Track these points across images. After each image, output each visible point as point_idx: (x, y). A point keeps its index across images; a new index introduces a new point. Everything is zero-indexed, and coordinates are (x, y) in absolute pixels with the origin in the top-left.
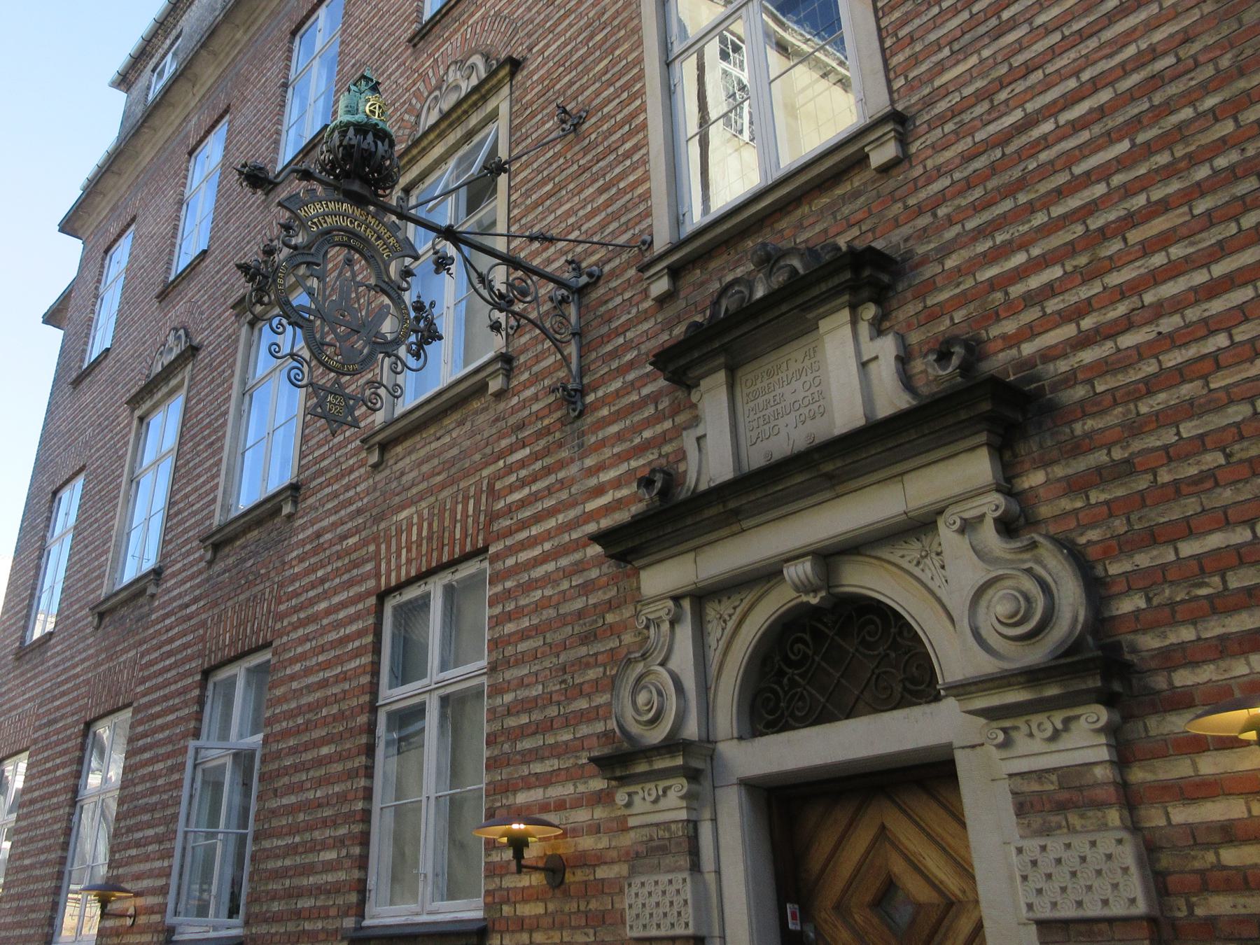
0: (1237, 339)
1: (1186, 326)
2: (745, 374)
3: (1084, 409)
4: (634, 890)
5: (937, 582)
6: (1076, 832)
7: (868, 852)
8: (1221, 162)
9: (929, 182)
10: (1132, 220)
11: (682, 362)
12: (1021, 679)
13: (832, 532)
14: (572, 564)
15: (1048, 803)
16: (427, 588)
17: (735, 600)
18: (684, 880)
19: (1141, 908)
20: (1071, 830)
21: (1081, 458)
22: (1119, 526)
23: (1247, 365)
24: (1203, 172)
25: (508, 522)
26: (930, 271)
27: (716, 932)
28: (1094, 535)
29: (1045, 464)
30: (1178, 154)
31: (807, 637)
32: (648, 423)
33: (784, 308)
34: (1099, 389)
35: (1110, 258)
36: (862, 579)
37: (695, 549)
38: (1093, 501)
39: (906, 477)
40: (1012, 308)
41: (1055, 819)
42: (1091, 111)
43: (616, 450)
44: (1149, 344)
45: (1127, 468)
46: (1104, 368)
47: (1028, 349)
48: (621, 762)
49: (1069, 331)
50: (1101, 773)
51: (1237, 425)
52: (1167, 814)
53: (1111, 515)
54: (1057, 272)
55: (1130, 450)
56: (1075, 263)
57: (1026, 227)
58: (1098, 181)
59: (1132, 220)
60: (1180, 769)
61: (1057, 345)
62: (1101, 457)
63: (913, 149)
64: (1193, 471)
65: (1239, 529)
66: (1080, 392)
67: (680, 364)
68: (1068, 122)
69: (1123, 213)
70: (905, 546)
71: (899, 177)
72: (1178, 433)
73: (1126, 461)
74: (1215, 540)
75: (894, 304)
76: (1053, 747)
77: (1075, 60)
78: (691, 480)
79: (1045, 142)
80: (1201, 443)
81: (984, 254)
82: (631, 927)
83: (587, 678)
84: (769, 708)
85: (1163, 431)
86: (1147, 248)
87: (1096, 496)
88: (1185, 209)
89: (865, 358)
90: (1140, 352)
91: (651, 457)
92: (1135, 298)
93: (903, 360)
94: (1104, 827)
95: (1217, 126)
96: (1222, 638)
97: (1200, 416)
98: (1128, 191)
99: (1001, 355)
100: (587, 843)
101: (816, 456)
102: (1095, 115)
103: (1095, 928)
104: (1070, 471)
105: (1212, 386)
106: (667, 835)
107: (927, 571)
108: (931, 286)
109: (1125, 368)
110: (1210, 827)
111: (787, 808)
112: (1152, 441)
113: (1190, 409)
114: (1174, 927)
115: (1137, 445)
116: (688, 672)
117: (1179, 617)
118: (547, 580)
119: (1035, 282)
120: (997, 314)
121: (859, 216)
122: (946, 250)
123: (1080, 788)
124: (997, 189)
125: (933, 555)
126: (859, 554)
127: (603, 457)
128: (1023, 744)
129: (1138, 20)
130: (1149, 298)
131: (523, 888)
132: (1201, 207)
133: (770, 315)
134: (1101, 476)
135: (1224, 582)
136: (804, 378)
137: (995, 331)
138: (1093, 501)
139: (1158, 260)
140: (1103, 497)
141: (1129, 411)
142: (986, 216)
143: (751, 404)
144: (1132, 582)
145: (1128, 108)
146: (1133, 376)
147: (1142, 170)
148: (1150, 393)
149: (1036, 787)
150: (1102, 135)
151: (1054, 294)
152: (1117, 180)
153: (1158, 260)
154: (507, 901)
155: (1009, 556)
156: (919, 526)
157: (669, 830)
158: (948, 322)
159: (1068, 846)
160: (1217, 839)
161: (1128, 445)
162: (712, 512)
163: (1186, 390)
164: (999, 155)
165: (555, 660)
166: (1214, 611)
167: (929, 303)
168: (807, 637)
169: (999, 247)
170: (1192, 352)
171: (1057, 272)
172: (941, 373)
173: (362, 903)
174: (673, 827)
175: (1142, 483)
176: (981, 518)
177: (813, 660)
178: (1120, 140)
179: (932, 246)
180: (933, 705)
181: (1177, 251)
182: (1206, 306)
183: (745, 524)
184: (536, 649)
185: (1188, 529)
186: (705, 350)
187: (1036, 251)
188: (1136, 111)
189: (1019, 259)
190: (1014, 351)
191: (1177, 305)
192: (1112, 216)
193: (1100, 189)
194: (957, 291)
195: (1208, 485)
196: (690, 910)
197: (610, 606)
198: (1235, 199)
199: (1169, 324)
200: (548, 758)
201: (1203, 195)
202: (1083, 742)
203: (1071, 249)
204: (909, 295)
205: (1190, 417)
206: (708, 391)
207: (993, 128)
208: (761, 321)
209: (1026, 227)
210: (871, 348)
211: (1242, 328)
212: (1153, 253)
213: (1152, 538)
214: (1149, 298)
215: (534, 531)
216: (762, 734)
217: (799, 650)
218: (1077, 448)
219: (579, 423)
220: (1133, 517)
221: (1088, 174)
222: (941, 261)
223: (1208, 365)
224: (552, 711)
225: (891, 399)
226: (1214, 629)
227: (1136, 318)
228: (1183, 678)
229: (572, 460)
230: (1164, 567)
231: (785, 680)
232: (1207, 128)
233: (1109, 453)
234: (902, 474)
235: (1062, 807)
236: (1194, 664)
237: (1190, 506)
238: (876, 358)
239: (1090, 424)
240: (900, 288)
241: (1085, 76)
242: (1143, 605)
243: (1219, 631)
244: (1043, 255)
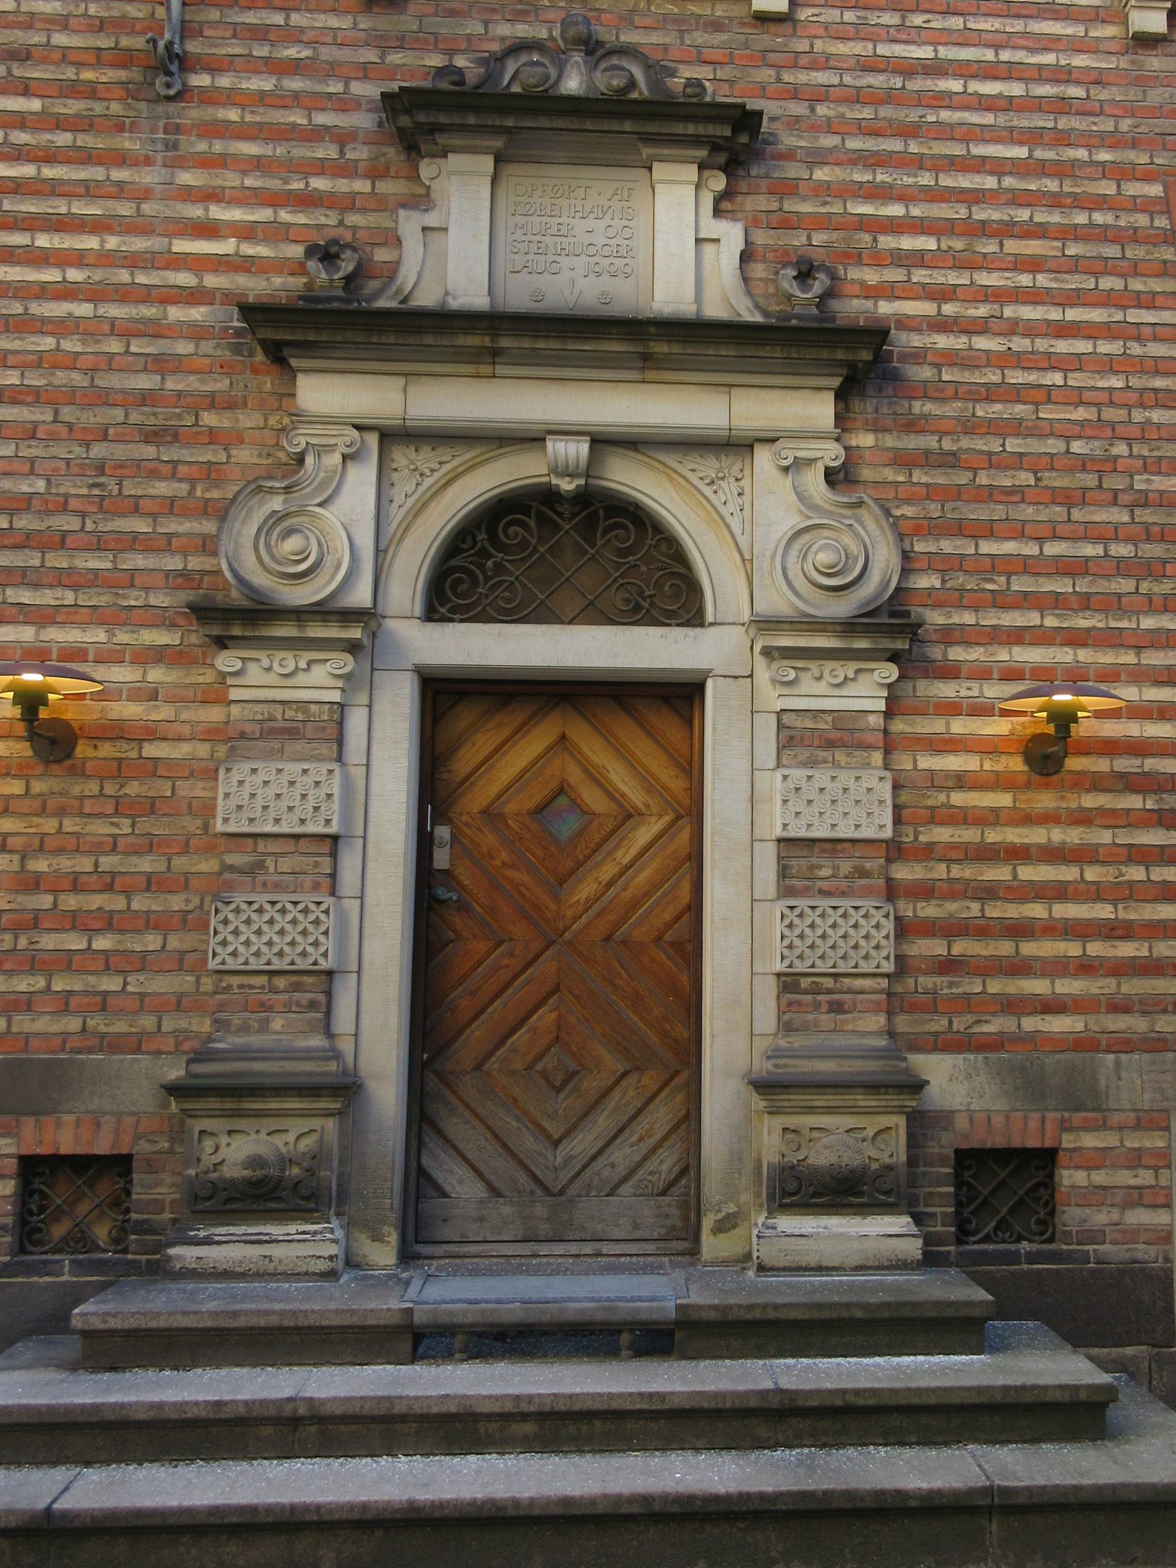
1: (1032, 353)
3: (926, 391)
4: (235, 777)
5: (731, 507)
7: (537, 760)
8: (1098, 218)
9: (813, 67)
10: (1007, 230)
11: (443, 119)
12: (838, 628)
13: (626, 420)
15: (807, 740)
17: (444, 453)
19: (888, 833)
20: (836, 765)
21: (913, 436)
22: (934, 509)
23: (1071, 408)
24: (1081, 218)
26: (793, 170)
27: (359, 831)
28: (909, 511)
30: (1066, 189)
31: (532, 523)
33: (628, 126)
34: (945, 377)
36: (629, 478)
38: (915, 480)
39: (734, 391)
40: (879, 260)
41: (821, 754)
42: (1000, 96)
45: (950, 461)
46: (951, 358)
47: (885, 308)
48: (234, 618)
49: (927, 308)
50: (872, 719)
51: (1052, 455)
52: (915, 761)
53: (928, 498)
54: (930, 243)
55: (960, 445)
56: (951, 243)
57: (911, 180)
59: (1007, 230)
60: (935, 726)
61: (914, 317)
62: (931, 442)
63: (803, 14)
64: (1007, 483)
65: (1031, 544)
66: (926, 373)
67: (425, 119)
68: (976, 93)
69: (1006, 218)
70: (699, 459)
71: (764, 39)
72: (1003, 445)
73: (953, 454)
74: (1010, 547)
75: (743, 186)
76: (837, 692)
77: (997, 31)
79: (942, 100)
80: (1019, 461)
82: (226, 820)
83: (152, 491)
84: (453, 591)
85: (991, 438)
87: (918, 476)
88: (1059, 244)
92: (996, 306)
94: (867, 765)
98: (1018, 199)
100: (130, 710)
101: (652, 330)
102: (1003, 103)
103: (839, 847)
104: (900, 445)
105: (1041, 415)
106: (300, 717)
107: (721, 493)
108: (787, 189)
110: (947, 774)
112: (979, 444)
114: (899, 849)
115: (966, 443)
117: (965, 602)
118: (62, 327)
119: (907, 243)
121: (716, 55)
122: (818, 158)
123: (852, 731)
124: (890, 121)
125: (732, 480)
126: (636, 450)
127: (219, 182)
128: (808, 685)
129: (1064, 32)
130: (1008, 312)
132: (1073, 250)
133: (605, 125)
134: (926, 459)
135: (1008, 583)
136: (607, 221)
137: (854, 273)
139: (1025, 280)
140: (925, 479)
141: (967, 409)
142: (870, 144)
143: (520, 220)
144: (935, 563)
145: (1035, 116)
146: (978, 378)
149: (810, 724)
150: (1005, 128)
151: (923, 265)
152: (1009, 182)
155: (827, 507)
156: (736, 446)
157: (306, 711)
159: (833, 778)
160: (950, 784)
161: (958, 440)
163: (1020, 409)
164: (899, 85)
166: (995, 605)
168: (532, 523)
169: (877, 187)
170: (1032, 378)
171: (930, 243)
172: (799, 293)
174: (313, 707)
175: (963, 478)
177: (535, 550)
178: (1021, 143)
180: (699, 629)
181: (1042, 280)
182: (1053, 342)
183: (500, 370)
185: (989, 531)
188: (1041, 124)
189: (895, 210)
190: (869, 304)
191: (1031, 330)
194: (822, 210)
195: (1015, 498)
196: (336, 806)
198: (1099, 257)
199: (1020, 344)
202: (864, 691)
205: (1017, 435)
207: (899, 50)
209: (911, 180)
211: (1076, 375)
212: (1023, 271)
213: (959, 529)
214: (1008, 312)
215: (43, 241)
216: (444, 619)
217: (517, 534)
218: (912, 426)
219: (172, 108)
220: (948, 506)
221: (984, 158)
222: (811, 165)
223: (1040, 395)
224: (70, 523)
225: (723, 296)
226: (991, 618)
228: (957, 654)
232: (1095, 179)
233: (940, 441)
235: (830, 744)
236: (969, 643)
237: (996, 512)
238: (717, 241)
239: (929, 407)
240: (754, 171)
241: (1005, 56)
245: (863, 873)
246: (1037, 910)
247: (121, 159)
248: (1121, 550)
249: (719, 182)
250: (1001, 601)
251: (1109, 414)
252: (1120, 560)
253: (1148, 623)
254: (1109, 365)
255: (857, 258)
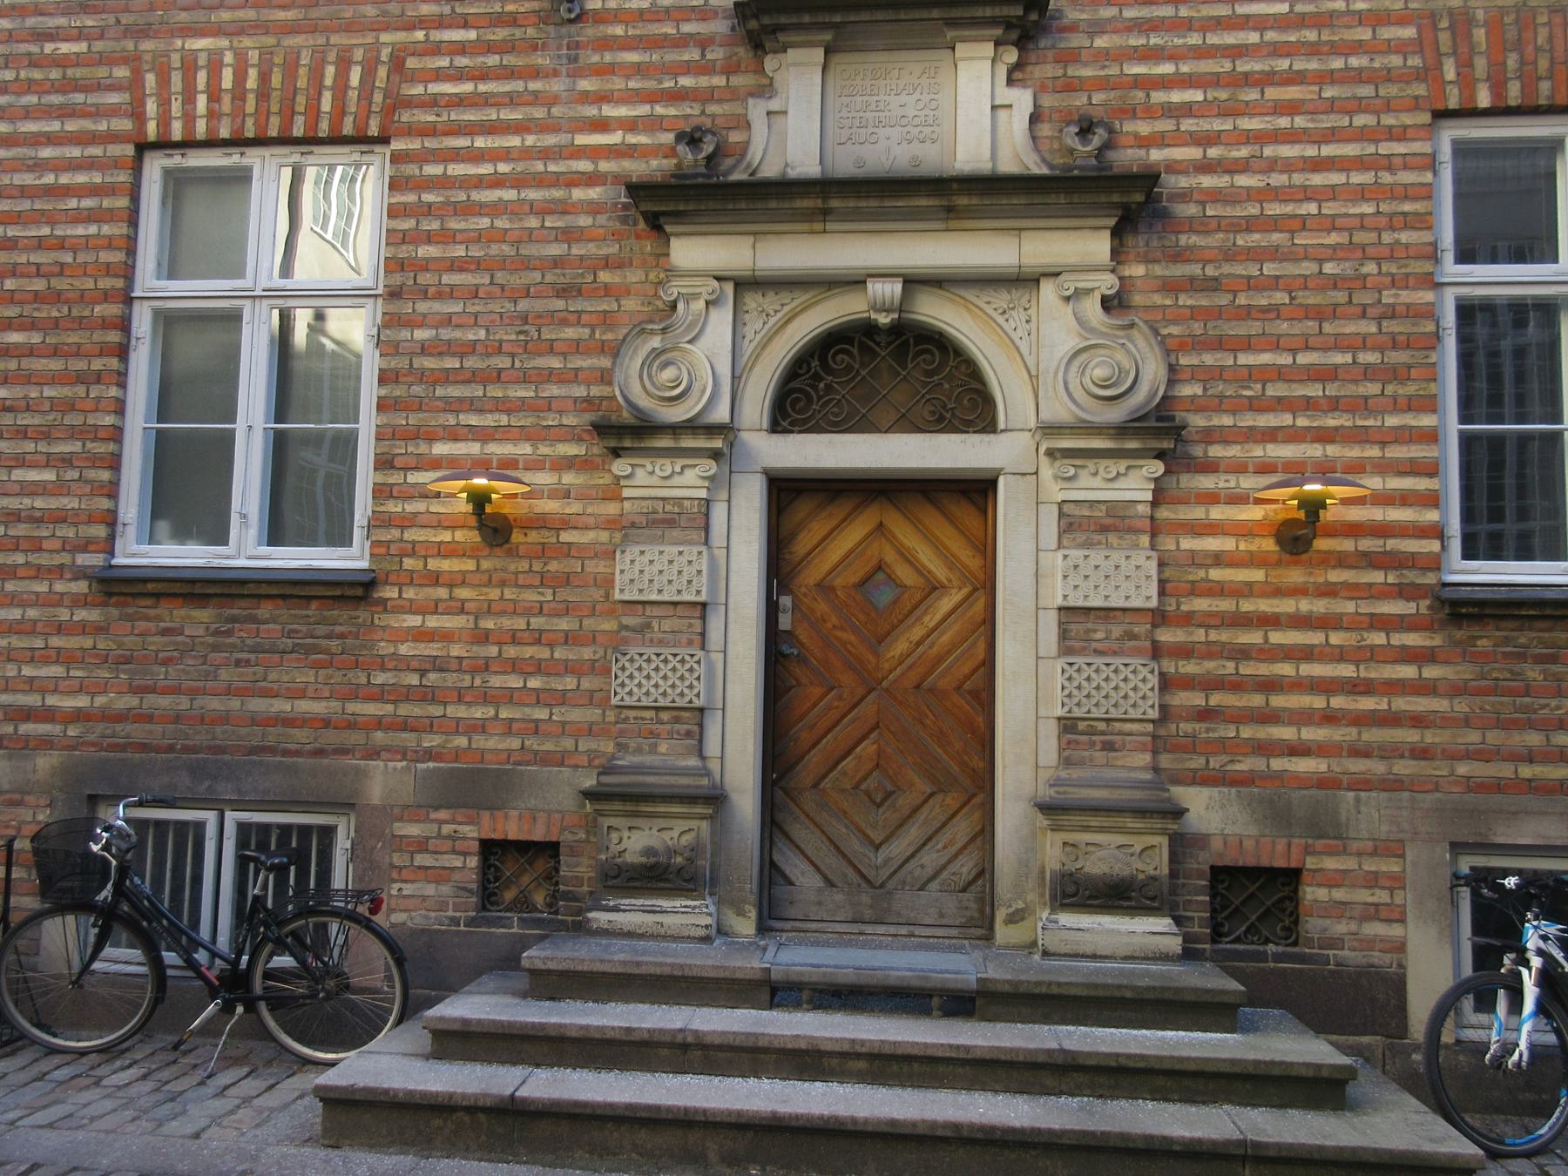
0: (1324, 211)
2: (836, 58)
3: (1191, 226)
5: (1020, 332)
6: (1112, 547)
8: (1354, 62)
10: (1269, 79)
14: (546, 201)
16: (245, 161)
17: (785, 296)
18: (700, 553)
19: (1154, 603)
20: (1109, 546)
21: (1179, 265)
22: (1197, 328)
24: (1337, 63)
25: (432, 118)
26: (1076, 41)
29: (1147, 260)
30: (1324, 38)
31: (855, 351)
32: (687, 68)
35: (1247, 103)
36: (936, 311)
37: (755, 234)
38: (1181, 303)
39: (1023, 234)
40: (1151, 113)
41: (1097, 537)
43: (632, 84)
44: (1259, 190)
46: (1215, 196)
47: (1156, 155)
48: (625, 433)
50: (1141, 509)
51: (1305, 277)
54: (1198, 96)
57: (1181, 41)
58: (1255, 29)
59: (1269, 79)
60: (1197, 513)
62: (1195, 269)
64: (1264, 302)
66: (1192, 210)
69: (1267, 68)
73: (1216, 279)
74: (1266, 358)
75: (1033, 58)
76: (1110, 485)
78: (755, 153)
80: (1275, 283)
81: (1135, 48)
82: (622, 591)
83: (562, 335)
84: (795, 405)
86: (1281, 108)
87: (1184, 300)
88: (1316, 88)
89: (997, 102)
90: (1250, 194)
91: (689, 111)
92: (1257, 147)
93: (1034, 119)
94: (1136, 546)
95: (1359, 29)
96: (1251, 428)
97: (1281, 261)
98: (1277, 50)
99: (1129, 151)
101: (955, 186)
104: (1167, 273)
106: (676, 510)
108: (1072, 57)
109: (1234, 202)
110: (1206, 553)
111: (788, 492)
112: (1239, 269)
113: (1274, 254)
115: (1227, 269)
116: (718, 353)
118: (495, 209)
119: (1177, 97)
120: (1134, 110)
122: (1097, 28)
123: (1123, 518)
127: (610, 86)
128: (1085, 479)
131: (440, 543)
132: (1328, 93)
136: (917, 95)
137: (1129, 127)
138: (1181, 303)
139: (1284, 122)
140: (1189, 302)
143: (846, 100)
146: (1238, 212)
147: (1293, 38)
148: (1248, 230)
149: (1086, 513)
152: (1270, 36)
153: (1284, 122)
154: (413, 554)
156: (1024, 281)
157: (680, 506)
158: (1085, 100)
160: (1209, 561)
162: (807, 203)
163: (1276, 238)
165: (509, 306)
166: (1251, 409)
167: (1070, 73)
170: (1289, 209)
172: (1080, 147)
173: (112, 538)
176: (1089, 291)
179: (1085, 16)
181: (1300, 122)
183: (829, 226)
184: (477, 287)
185: (1247, 345)
186: (820, 19)
187: (1185, 68)
189: (1167, 68)
190: (1142, 152)
191: (1288, 166)
192: (1258, 67)
193: (1253, 37)
194: (1102, 73)
195: (1272, 315)
197: (607, 263)
199: (1278, 179)
200: (491, 411)
201: (1333, 82)
202: (1134, 485)
203: (1215, 81)
204: (1050, 54)
205: (1273, 260)
206: (795, 64)
208: (902, 16)
209: (1181, 41)
210: (1006, 95)
211: (1330, 204)
212: (1282, 115)
213: (1220, 344)
219: (573, 28)
221: (1247, 17)
222: (1092, 35)
223: (1296, 224)
226: (1248, 420)
227: (1254, 163)
228: (1216, 451)
229: (556, 73)
230: (1222, 367)
231: (822, 385)
232: (1351, 27)
234: (1020, 230)
235: (1104, 529)
236: (1226, 442)
237: (1254, 328)
239: (1194, 239)
240: (1042, 44)
242: (1200, 392)
243: (1250, 423)
244: (1190, 75)
245: (1133, 636)
246: (1286, 669)
247: (536, 73)
248: (1371, 358)
249: (1012, 56)
250: (1255, 405)
251: (1360, 237)
252: (1367, 366)
253: (1392, 421)
254: (1361, 193)
255: (1132, 113)
